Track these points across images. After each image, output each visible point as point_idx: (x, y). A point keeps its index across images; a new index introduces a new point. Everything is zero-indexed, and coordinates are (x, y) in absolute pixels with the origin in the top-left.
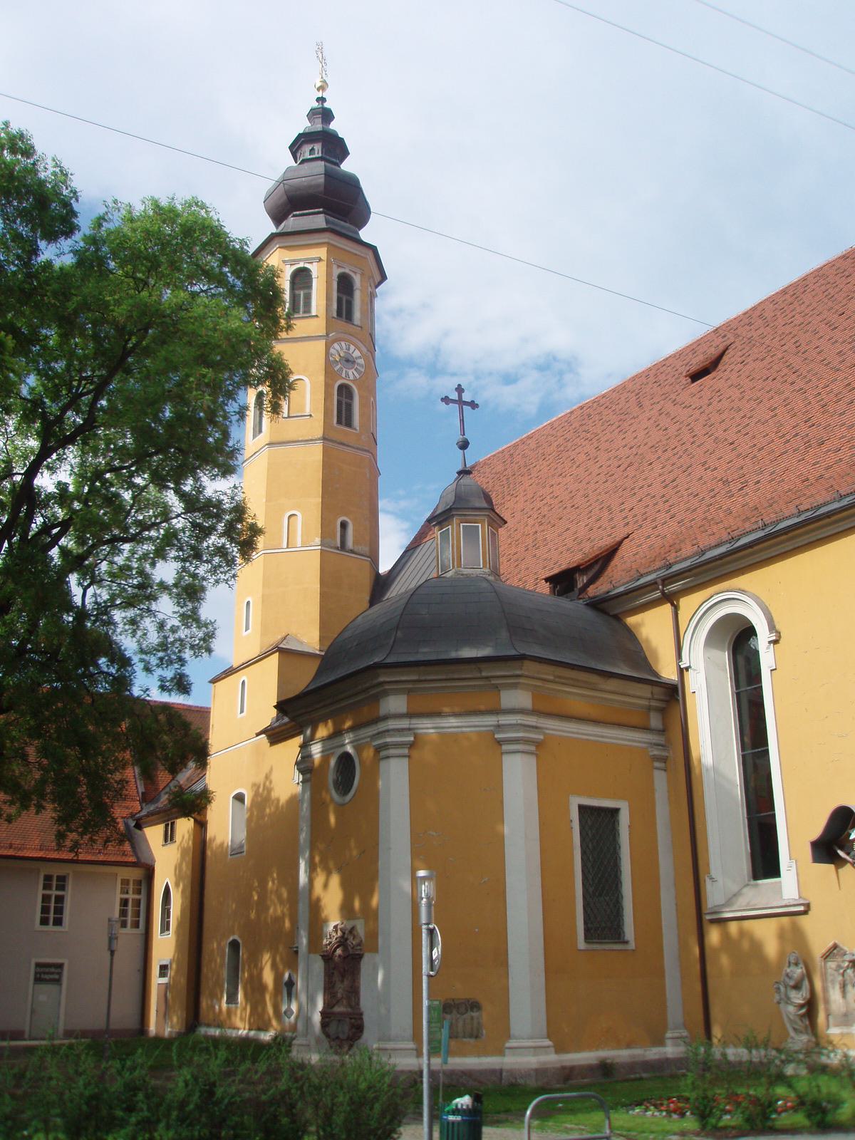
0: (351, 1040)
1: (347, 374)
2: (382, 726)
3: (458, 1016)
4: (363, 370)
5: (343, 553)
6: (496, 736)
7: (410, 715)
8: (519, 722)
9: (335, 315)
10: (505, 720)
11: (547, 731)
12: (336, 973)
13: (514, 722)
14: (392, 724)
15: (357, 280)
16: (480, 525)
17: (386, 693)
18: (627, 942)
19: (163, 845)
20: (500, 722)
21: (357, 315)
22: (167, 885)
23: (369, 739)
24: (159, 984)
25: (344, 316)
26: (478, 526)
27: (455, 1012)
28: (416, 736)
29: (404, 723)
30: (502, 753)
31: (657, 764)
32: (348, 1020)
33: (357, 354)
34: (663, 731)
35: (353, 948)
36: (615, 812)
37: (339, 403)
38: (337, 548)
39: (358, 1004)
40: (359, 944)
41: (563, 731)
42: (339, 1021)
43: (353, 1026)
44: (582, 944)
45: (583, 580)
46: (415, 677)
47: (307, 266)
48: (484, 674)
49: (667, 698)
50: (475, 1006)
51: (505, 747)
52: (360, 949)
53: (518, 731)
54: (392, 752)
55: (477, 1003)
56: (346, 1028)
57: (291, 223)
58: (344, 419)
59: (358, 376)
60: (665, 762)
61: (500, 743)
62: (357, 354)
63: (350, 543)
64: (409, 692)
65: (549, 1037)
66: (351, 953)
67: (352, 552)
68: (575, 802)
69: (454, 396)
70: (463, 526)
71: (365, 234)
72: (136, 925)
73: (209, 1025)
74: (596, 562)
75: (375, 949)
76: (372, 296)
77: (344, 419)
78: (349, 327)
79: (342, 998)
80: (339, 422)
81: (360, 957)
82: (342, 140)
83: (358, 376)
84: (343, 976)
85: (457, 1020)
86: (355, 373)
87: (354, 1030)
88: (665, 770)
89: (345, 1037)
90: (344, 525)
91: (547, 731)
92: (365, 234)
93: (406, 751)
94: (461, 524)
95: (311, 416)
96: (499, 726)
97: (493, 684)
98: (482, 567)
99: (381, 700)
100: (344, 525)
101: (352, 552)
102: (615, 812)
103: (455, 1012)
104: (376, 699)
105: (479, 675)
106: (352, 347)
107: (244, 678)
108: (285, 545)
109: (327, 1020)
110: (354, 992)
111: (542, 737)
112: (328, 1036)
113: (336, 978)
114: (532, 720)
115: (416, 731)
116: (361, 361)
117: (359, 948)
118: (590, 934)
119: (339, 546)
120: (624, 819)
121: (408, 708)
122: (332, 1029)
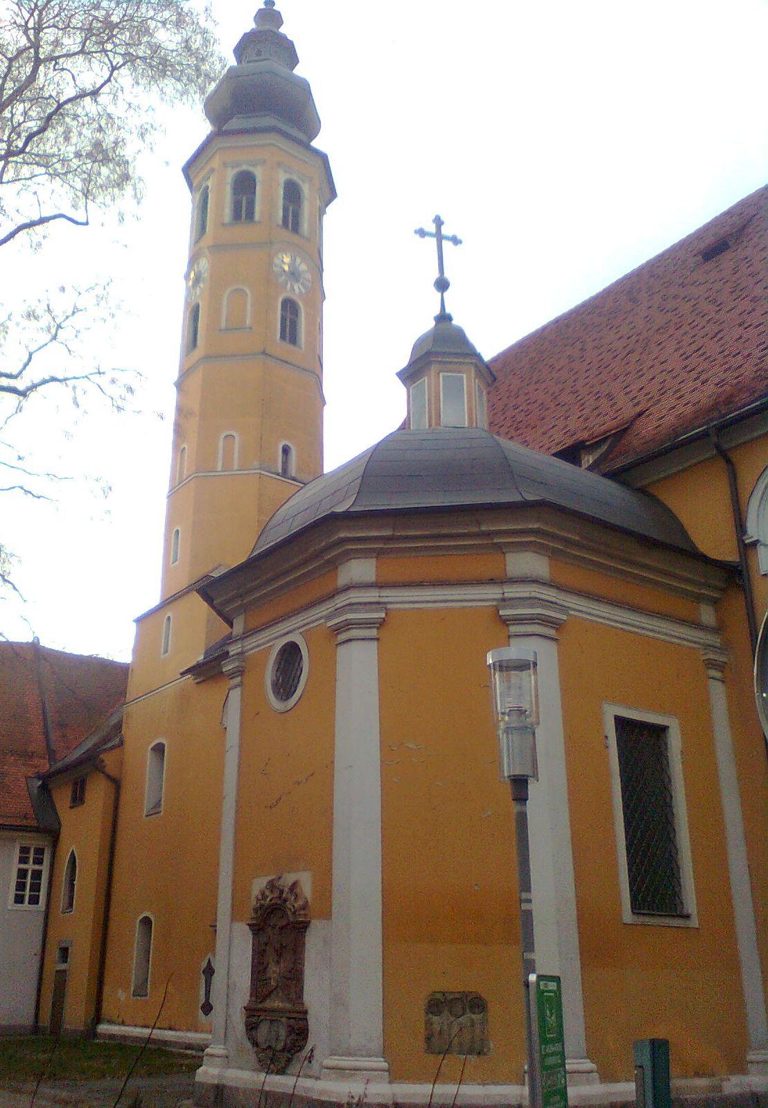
0: (289, 1052)
1: (292, 287)
2: (341, 601)
3: (452, 1019)
4: (310, 285)
5: (284, 479)
6: (501, 613)
7: (379, 585)
8: (533, 595)
9: (280, 222)
10: (512, 591)
11: (572, 612)
12: (270, 950)
13: (527, 595)
14: (355, 596)
15: (306, 189)
16: (465, 376)
17: (347, 556)
18: (688, 917)
19: (71, 808)
20: (506, 595)
21: (305, 226)
22: (73, 853)
23: (323, 621)
24: (57, 971)
25: (288, 338)
26: (462, 377)
27: (446, 1012)
28: (387, 611)
29: (372, 595)
30: (509, 637)
31: (713, 673)
32: (284, 1020)
33: (303, 267)
34: (717, 630)
35: (294, 913)
36: (663, 729)
37: (283, 319)
38: (278, 474)
39: (300, 995)
40: (304, 907)
41: (593, 615)
42: (272, 1021)
43: (291, 1030)
44: (628, 916)
45: (588, 460)
46: (387, 532)
47: (251, 169)
48: (484, 528)
49: (724, 586)
50: (477, 1004)
51: (514, 629)
52: (305, 915)
53: (532, 607)
54: (355, 633)
55: (480, 998)
56: (283, 1033)
57: (234, 124)
58: (288, 335)
59: (303, 291)
60: (722, 672)
61: (505, 622)
62: (303, 267)
63: (293, 471)
64: (379, 553)
65: (384, 1055)
66: (291, 919)
67: (294, 479)
68: (611, 711)
69: (432, 228)
70: (443, 376)
71: (315, 143)
72: (34, 900)
73: (111, 1022)
74: (605, 440)
75: (327, 915)
76: (322, 212)
77: (288, 335)
78: (295, 238)
79: (277, 987)
80: (283, 337)
81: (305, 926)
82: (291, 43)
83: (303, 291)
84: (279, 954)
85: (450, 1025)
86: (301, 287)
87: (293, 1036)
88: (723, 682)
89: (280, 1046)
90: (286, 451)
91: (572, 612)
92: (315, 143)
93: (374, 633)
94: (441, 375)
95: (251, 328)
96: (503, 600)
97: (496, 544)
98: (466, 426)
99: (340, 568)
100: (286, 451)
101: (294, 479)
102: (663, 729)
103: (446, 1012)
104: (333, 565)
105: (476, 530)
106: (298, 260)
107: (169, 614)
108: (219, 466)
109: (254, 1020)
110: (295, 977)
111: (565, 617)
112: (255, 1044)
113: (271, 957)
114: (550, 594)
115: (389, 606)
116: (308, 276)
117: (302, 912)
118: (638, 905)
119: (280, 471)
120: (675, 741)
121: (377, 575)
122: (263, 1033)
